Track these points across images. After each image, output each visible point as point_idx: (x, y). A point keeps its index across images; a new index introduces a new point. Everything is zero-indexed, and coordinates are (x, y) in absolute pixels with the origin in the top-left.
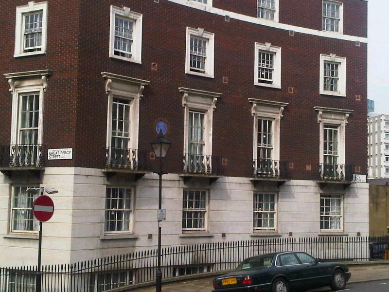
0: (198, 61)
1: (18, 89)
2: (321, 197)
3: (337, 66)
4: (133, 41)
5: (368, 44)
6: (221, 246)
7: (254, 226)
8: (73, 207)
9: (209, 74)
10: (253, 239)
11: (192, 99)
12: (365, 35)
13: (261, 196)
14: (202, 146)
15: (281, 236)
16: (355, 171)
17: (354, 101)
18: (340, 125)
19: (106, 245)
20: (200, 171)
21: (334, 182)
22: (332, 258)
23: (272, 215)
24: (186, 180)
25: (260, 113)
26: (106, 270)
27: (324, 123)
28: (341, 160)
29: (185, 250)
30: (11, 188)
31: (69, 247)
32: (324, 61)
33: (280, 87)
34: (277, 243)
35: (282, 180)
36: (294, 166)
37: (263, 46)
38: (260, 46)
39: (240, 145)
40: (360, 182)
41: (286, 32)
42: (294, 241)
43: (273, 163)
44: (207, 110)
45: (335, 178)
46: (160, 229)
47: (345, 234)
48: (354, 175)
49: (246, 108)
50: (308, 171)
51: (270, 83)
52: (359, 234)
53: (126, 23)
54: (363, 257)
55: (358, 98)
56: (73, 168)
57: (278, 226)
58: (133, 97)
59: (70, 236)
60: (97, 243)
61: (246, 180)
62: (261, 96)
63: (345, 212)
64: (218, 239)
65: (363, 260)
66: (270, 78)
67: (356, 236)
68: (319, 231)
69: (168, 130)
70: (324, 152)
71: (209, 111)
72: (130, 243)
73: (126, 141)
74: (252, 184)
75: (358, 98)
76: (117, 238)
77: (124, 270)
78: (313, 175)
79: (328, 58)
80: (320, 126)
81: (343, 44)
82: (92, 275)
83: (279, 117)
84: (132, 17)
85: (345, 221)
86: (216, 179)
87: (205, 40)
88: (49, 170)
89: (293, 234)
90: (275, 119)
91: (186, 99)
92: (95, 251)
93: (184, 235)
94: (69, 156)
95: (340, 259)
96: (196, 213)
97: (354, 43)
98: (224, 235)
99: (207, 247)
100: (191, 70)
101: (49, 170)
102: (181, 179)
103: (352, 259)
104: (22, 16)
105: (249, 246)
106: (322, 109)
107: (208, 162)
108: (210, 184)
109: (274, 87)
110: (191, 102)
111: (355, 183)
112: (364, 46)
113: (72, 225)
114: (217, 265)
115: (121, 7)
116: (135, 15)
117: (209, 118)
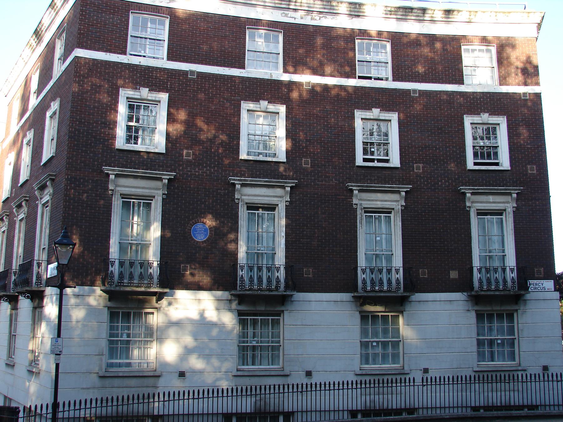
2: (239, 316)
3: (494, 129)
6: (301, 389)
10: (359, 379)
15: (408, 374)
16: (534, 275)
17: (527, 174)
18: (505, 210)
19: (108, 382)
20: (377, 288)
21: (492, 293)
22: (499, 404)
24: (241, 299)
27: (477, 210)
30: (35, 312)
32: (471, 124)
33: (399, 166)
34: (403, 384)
35: (288, 293)
37: (368, 114)
38: (363, 113)
40: (544, 290)
44: (278, 205)
45: (377, 288)
46: (57, 366)
47: (520, 368)
49: (343, 197)
50: (454, 279)
51: (497, 164)
52: (545, 368)
54: (443, 405)
55: (532, 170)
58: (153, 195)
61: (346, 296)
62: (367, 180)
64: (298, 378)
65: (451, 410)
67: (539, 371)
68: (475, 365)
72: (151, 381)
74: (471, 300)
75: (532, 169)
76: (124, 375)
79: (476, 119)
85: (521, 350)
89: (430, 371)
90: (393, 209)
91: (239, 191)
92: (91, 391)
93: (239, 373)
95: (514, 406)
97: (408, 91)
98: (309, 374)
99: (282, 389)
102: (233, 298)
106: (470, 189)
109: (392, 166)
114: (300, 414)
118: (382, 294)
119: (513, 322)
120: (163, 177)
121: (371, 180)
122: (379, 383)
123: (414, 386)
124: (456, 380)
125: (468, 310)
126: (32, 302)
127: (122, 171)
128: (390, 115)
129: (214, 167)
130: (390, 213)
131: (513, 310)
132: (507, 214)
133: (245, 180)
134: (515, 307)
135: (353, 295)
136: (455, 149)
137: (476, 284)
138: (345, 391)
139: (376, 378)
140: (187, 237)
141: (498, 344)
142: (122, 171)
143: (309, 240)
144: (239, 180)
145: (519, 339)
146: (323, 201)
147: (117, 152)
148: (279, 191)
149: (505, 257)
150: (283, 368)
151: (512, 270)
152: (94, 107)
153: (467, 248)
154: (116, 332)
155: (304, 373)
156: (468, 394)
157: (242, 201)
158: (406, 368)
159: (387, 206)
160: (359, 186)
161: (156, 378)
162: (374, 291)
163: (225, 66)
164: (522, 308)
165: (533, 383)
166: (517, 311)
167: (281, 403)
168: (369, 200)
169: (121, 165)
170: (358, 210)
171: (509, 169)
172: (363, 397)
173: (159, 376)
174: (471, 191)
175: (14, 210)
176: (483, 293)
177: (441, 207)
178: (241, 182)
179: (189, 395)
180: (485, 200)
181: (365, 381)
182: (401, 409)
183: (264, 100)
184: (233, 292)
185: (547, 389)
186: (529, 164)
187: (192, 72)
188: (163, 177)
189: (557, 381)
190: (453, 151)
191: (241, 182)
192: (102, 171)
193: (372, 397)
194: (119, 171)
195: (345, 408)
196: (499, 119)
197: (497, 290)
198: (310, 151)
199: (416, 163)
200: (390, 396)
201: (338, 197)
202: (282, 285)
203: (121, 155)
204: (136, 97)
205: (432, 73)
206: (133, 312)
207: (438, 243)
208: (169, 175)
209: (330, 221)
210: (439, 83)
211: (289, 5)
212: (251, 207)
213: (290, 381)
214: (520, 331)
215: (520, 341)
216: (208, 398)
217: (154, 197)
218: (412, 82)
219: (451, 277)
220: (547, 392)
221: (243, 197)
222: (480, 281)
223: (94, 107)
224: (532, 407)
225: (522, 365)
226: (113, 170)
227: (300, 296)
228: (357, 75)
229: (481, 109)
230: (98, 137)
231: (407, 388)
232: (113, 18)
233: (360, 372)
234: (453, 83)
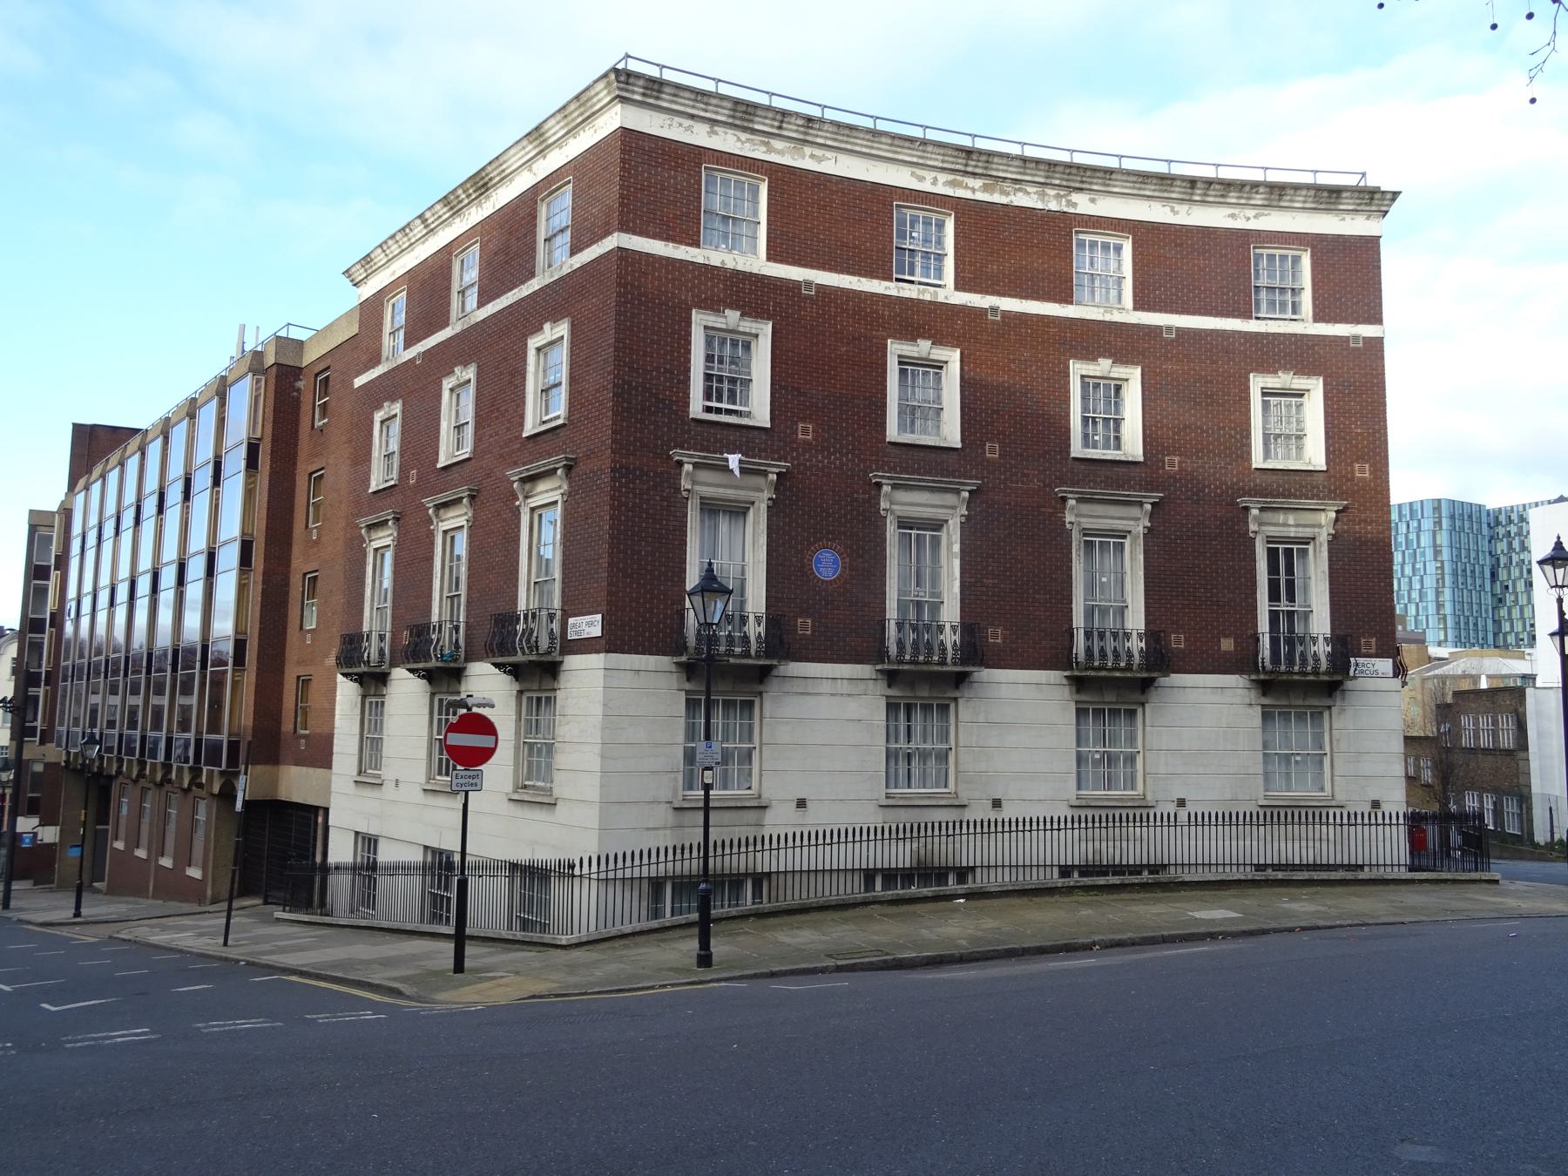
0: (725, 386)
1: (530, 500)
4: (751, 380)
5: (1385, 341)
6: (988, 828)
7: (887, 787)
8: (602, 738)
9: (949, 438)
10: (1077, 813)
11: (902, 496)
12: (1376, 318)
13: (710, 705)
14: (1122, 611)
17: (1352, 479)
18: (1314, 539)
20: (921, 658)
21: (1093, 673)
23: (1131, 759)
24: (891, 678)
26: (686, 872)
27: (1267, 537)
28: (1320, 623)
29: (899, 834)
31: (594, 823)
36: (1186, 640)
37: (1091, 367)
38: (1084, 366)
39: (1037, 596)
41: (1155, 331)
42: (1172, 819)
43: (751, 618)
44: (947, 521)
45: (921, 658)
47: (1334, 803)
48: (1352, 659)
49: (1050, 510)
52: (1376, 804)
53: (734, 344)
55: (1362, 472)
56: (602, 655)
57: (1148, 783)
58: (752, 499)
59: (597, 798)
60: (663, 815)
61: (1055, 676)
62: (1089, 481)
63: (1335, 750)
64: (980, 812)
65: (1228, 869)
67: (1367, 809)
69: (844, 568)
71: (950, 522)
72: (751, 816)
73: (936, 607)
77: (739, 874)
78: (1242, 662)
80: (1257, 544)
81: (1314, 345)
82: (657, 884)
83: (1141, 528)
84: (748, 330)
85: (1336, 773)
86: (1152, 680)
87: (747, 338)
88: (573, 662)
90: (1130, 532)
93: (891, 802)
94: (596, 631)
98: (997, 804)
99: (953, 830)
100: (708, 410)
101: (573, 662)
102: (879, 677)
103: (1361, 867)
104: (538, 354)
105: (1010, 832)
107: (953, 638)
108: (957, 687)
110: (902, 504)
111: (1355, 677)
112: (1376, 345)
113: (601, 776)
115: (719, 311)
116: (754, 325)
117: (952, 541)
118: (1118, 674)
120: (769, 469)
121: (1095, 482)
122: (1093, 822)
123: (1175, 826)
124: (1229, 820)
125: (1251, 705)
126: (517, 680)
127: (705, 458)
128: (1128, 370)
129: (847, 453)
130: (1124, 537)
131: (949, 698)
133: (897, 478)
134: (1328, 702)
135: (1067, 673)
136: (1233, 432)
137: (893, 649)
138: (1014, 834)
139: (1104, 813)
140: (805, 573)
141: (1296, 762)
142: (705, 458)
143: (996, 581)
144: (889, 478)
145: (1332, 755)
146: (1019, 517)
147: (692, 424)
148: (950, 499)
150: (956, 793)
151: (758, 620)
152: (653, 342)
153: (1250, 600)
155: (990, 802)
156: (1248, 843)
157: (892, 512)
158: (1149, 797)
159: (1120, 527)
160: (1077, 493)
161: (762, 811)
162: (917, 663)
163: (860, 275)
164: (1338, 704)
165: (1296, 827)
166: (1329, 707)
167: (929, 853)
168: (1092, 516)
169: (699, 447)
172: (1083, 845)
173: (766, 807)
174: (1076, 496)
175: (431, 511)
176: (732, 660)
178: (892, 482)
179: (883, 834)
181: (1080, 817)
182: (1141, 866)
183: (924, 338)
184: (1253, 677)
185: (1227, 838)
186: (1357, 461)
187: (808, 284)
188: (769, 469)
189: (1377, 825)
190: (1231, 436)
191: (892, 482)
192: (670, 457)
193: (1097, 844)
194: (700, 457)
195: (1056, 863)
196: (1309, 381)
197: (1316, 672)
199: (1168, 455)
200: (1124, 844)
201: (1043, 510)
203: (699, 429)
204: (718, 326)
205: (1199, 297)
206: (1093, 710)
208: (778, 466)
209: (1030, 550)
211: (1192, 194)
212: (904, 523)
213: (968, 815)
214: (1335, 742)
215: (1335, 759)
216: (854, 842)
217: (753, 503)
218: (1166, 312)
220: (1374, 844)
221: (894, 507)
222: (901, 644)
223: (653, 342)
224: (1155, 869)
225: (763, 796)
226: (691, 456)
227: (986, 674)
228: (895, 276)
229: (1280, 363)
230: (661, 397)
231: (1145, 829)
232: (675, 178)
233: (885, 802)
234: (1234, 316)
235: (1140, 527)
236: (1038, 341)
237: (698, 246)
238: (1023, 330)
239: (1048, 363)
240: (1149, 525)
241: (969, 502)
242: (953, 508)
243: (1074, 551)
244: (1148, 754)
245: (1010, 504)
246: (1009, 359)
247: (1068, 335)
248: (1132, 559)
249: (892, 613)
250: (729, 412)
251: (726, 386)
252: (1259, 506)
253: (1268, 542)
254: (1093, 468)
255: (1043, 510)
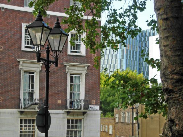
2: (71, 120)
18: (81, 74)
24: (22, 113)
25: (25, 68)
28: (82, 97)
39: (11, 89)
40: (95, 110)
48: (89, 106)
51: (79, 52)
66: (79, 49)
70: (24, 90)
90: (36, 71)
96: (76, 132)
119: (81, 123)
121: (27, 57)
132: (83, 75)
149: (80, 94)
154: (22, 125)
166: (83, 118)
170: (21, 71)
171: (85, 55)
177: (55, 71)
180: (77, 69)
198: (3, 42)
201: (13, 65)
202: (83, 107)
207: (53, 87)
210: (59, 12)
214: (84, 127)
219: (58, 103)
235: (84, 72)
236: (14, 17)
237: (23, 7)
238: (10, 14)
239: (16, 23)
240: (41, 69)
241: (87, 70)
242: (38, 68)
243: (21, 76)
244: (84, 131)
245: (5, 63)
246: (6, 22)
247: (22, 16)
248: (36, 79)
249: (22, 96)
250: (76, 52)
251: (78, 46)
252: (69, 65)
253: (71, 74)
254: (27, 53)
255: (13, 65)
